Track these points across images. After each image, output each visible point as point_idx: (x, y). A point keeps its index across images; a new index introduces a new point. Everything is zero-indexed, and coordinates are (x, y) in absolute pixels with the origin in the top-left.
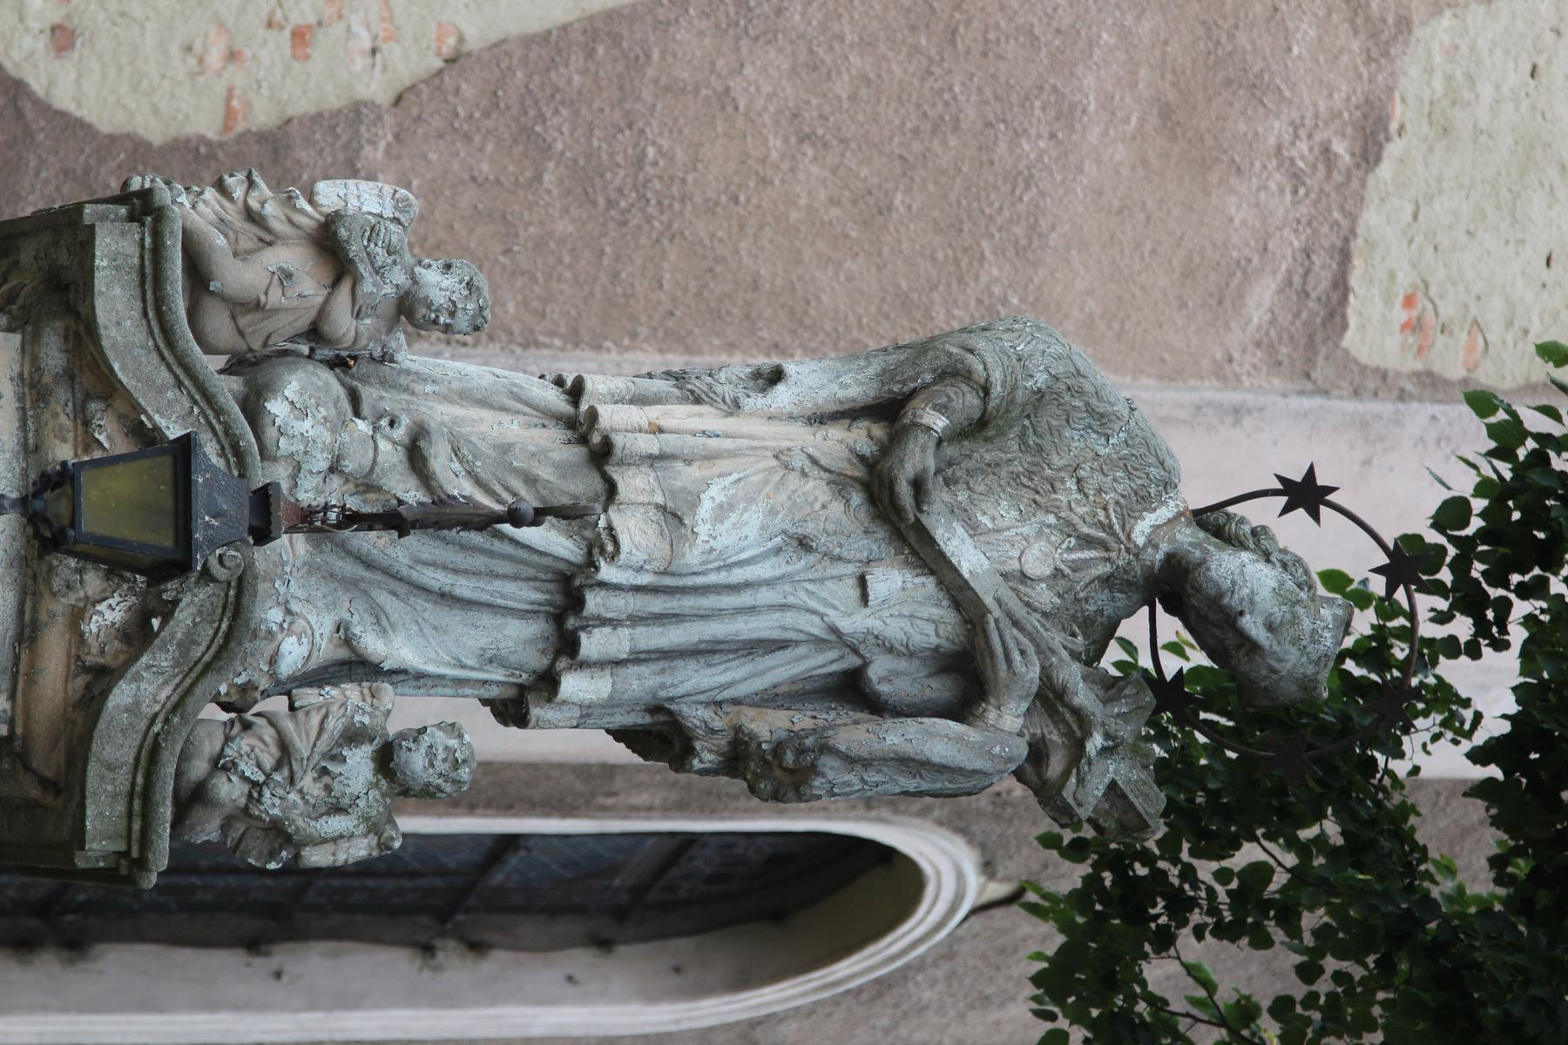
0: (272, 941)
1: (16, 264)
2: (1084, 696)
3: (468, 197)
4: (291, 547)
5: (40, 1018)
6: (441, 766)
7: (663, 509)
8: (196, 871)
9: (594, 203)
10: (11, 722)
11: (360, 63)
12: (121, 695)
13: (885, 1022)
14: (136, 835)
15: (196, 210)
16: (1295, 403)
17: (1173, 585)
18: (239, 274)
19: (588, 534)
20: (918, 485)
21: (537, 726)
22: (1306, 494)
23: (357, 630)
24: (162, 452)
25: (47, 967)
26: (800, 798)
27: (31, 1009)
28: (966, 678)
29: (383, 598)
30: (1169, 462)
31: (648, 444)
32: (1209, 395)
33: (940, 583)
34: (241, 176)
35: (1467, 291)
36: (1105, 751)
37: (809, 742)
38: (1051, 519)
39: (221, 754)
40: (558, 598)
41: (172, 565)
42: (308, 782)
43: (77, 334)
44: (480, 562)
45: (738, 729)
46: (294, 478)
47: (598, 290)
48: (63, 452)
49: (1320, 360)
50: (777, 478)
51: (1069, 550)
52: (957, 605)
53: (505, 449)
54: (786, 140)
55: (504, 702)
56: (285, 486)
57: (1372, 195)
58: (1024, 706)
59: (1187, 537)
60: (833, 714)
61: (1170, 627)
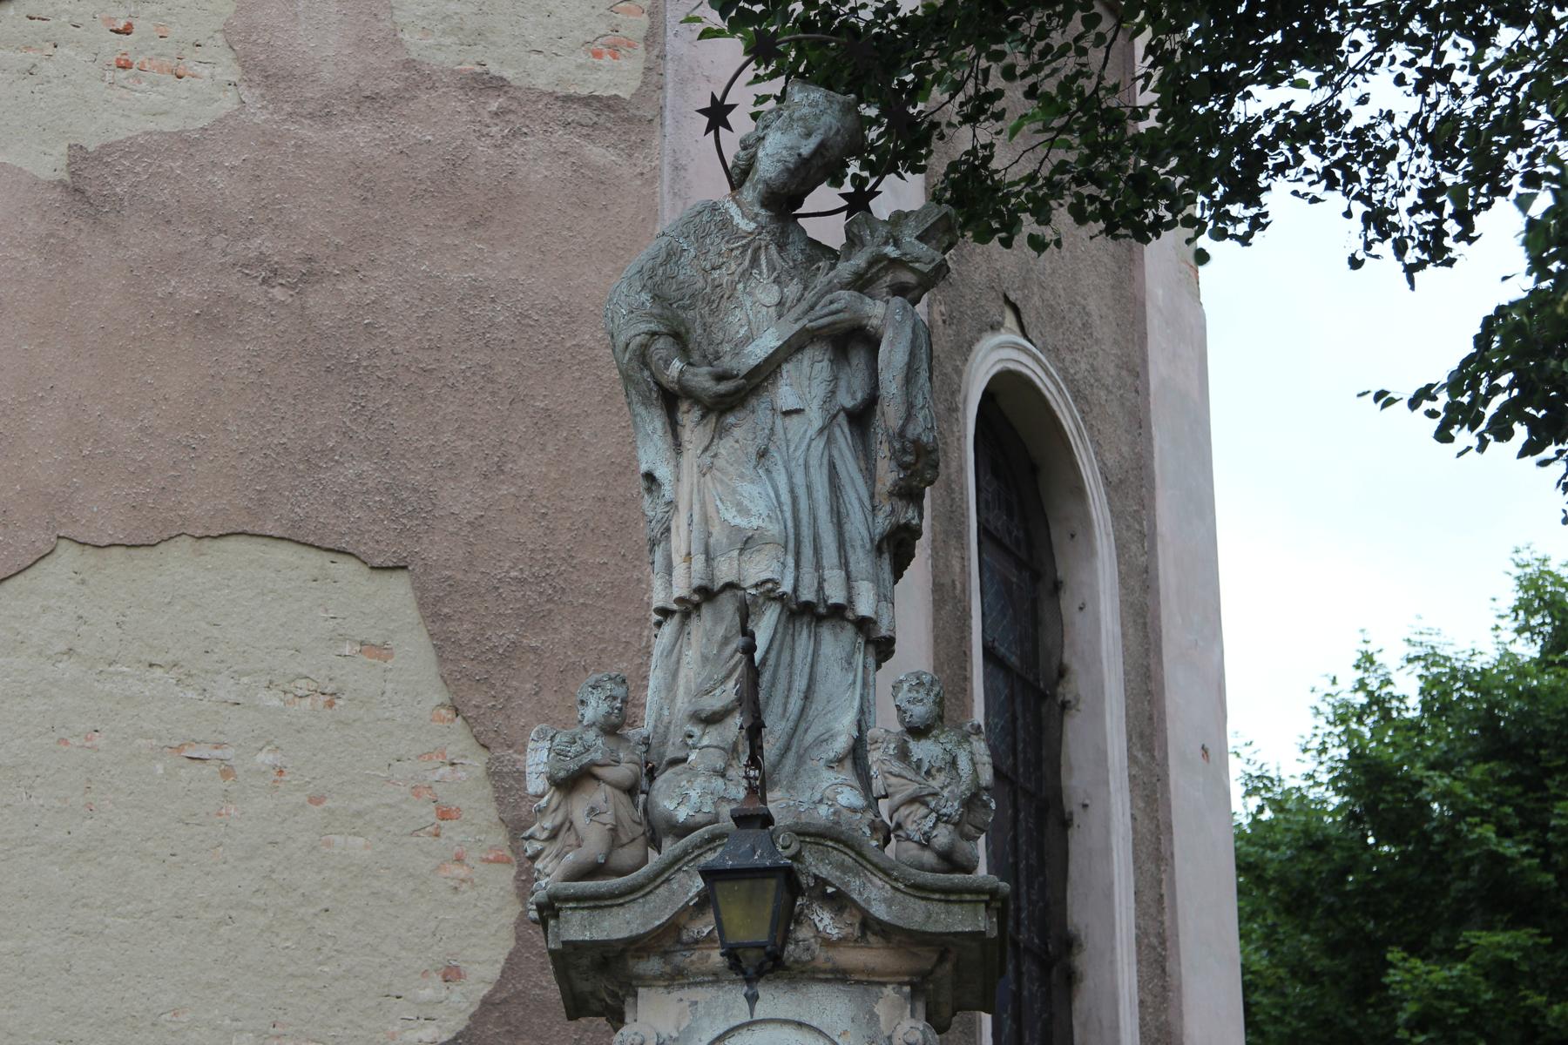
0: (1062, 811)
1: (592, 993)
2: (860, 260)
3: (548, 696)
4: (777, 802)
5: (1119, 965)
6: (922, 694)
7: (742, 550)
8: (1016, 864)
9: (550, 611)
10: (901, 984)
11: (461, 774)
12: (880, 911)
13: (1103, 393)
14: (974, 897)
15: (551, 875)
16: (668, 129)
17: (783, 202)
18: (593, 845)
19: (761, 601)
20: (720, 377)
21: (893, 631)
22: (717, 114)
23: (832, 755)
24: (713, 890)
25: (1082, 962)
26: (935, 450)
27: (1113, 972)
28: (849, 341)
29: (809, 738)
30: (699, 208)
31: (699, 562)
32: (665, 188)
33: (786, 360)
34: (526, 844)
35: (589, 15)
36: (897, 244)
37: (897, 446)
38: (740, 286)
39: (919, 843)
40: (806, 619)
41: (789, 879)
42: (935, 784)
43: (637, 950)
44: (783, 673)
45: (891, 494)
46: (730, 801)
47: (609, 607)
48: (716, 957)
49: (641, 113)
50: (718, 474)
51: (761, 273)
52: (800, 348)
53: (705, 659)
54: (503, 482)
55: (878, 653)
56: (734, 806)
57: (525, 82)
58: (867, 300)
59: (749, 194)
60: (879, 430)
61: (810, 203)
